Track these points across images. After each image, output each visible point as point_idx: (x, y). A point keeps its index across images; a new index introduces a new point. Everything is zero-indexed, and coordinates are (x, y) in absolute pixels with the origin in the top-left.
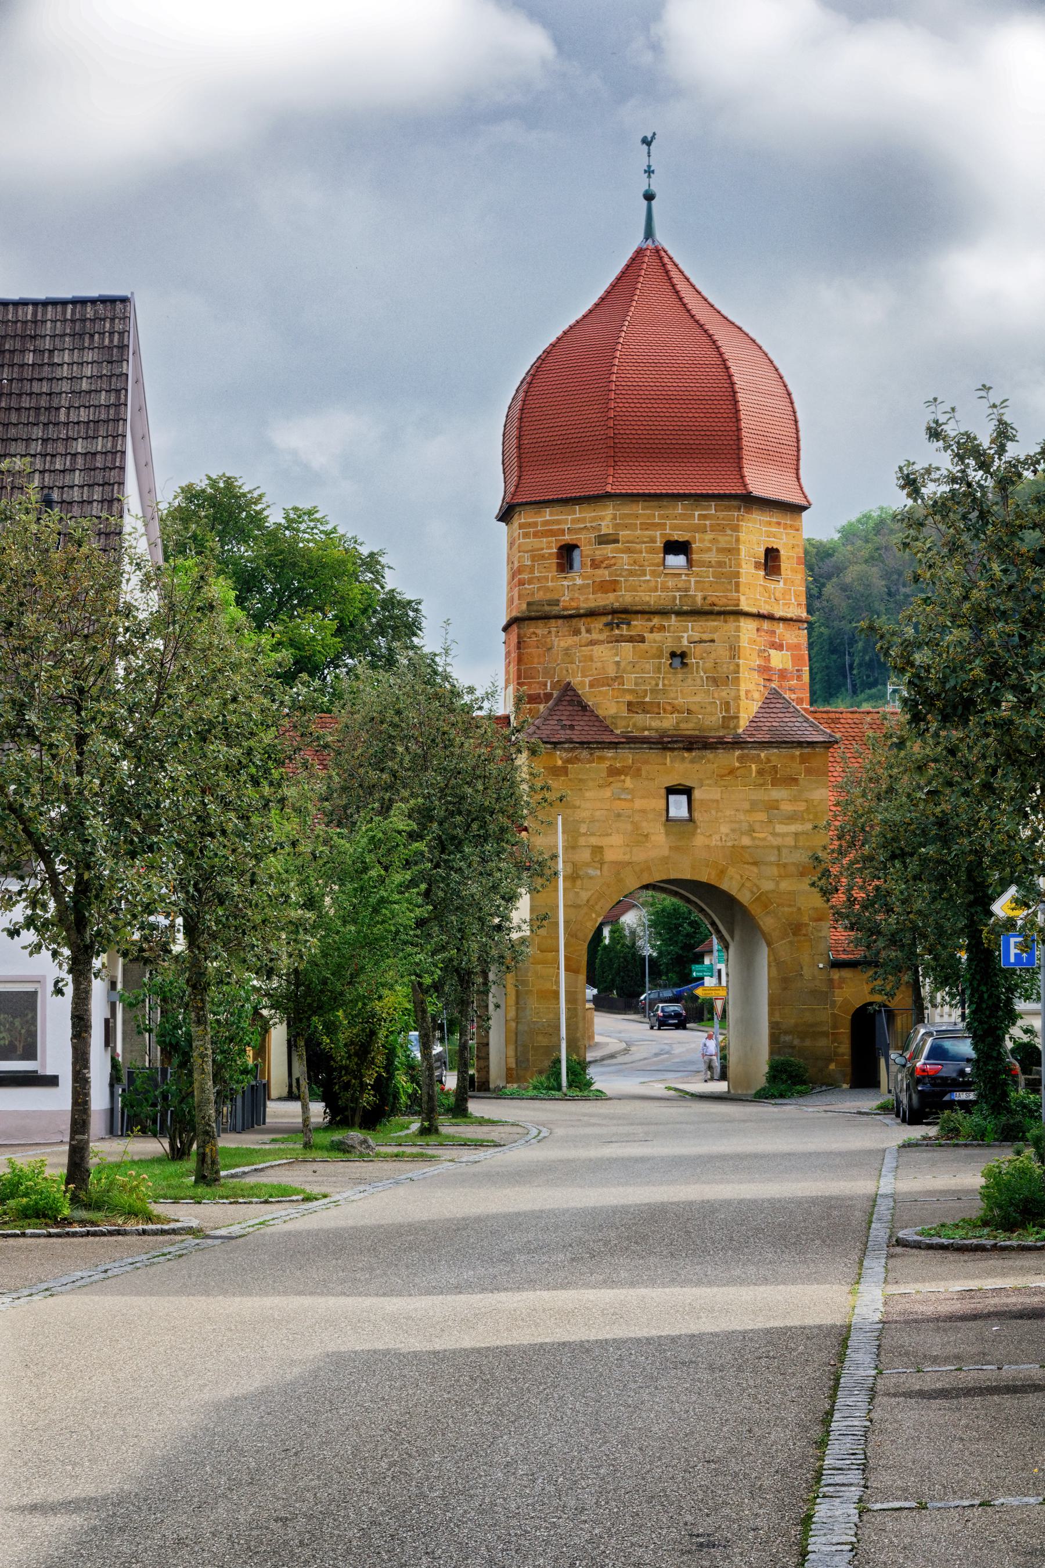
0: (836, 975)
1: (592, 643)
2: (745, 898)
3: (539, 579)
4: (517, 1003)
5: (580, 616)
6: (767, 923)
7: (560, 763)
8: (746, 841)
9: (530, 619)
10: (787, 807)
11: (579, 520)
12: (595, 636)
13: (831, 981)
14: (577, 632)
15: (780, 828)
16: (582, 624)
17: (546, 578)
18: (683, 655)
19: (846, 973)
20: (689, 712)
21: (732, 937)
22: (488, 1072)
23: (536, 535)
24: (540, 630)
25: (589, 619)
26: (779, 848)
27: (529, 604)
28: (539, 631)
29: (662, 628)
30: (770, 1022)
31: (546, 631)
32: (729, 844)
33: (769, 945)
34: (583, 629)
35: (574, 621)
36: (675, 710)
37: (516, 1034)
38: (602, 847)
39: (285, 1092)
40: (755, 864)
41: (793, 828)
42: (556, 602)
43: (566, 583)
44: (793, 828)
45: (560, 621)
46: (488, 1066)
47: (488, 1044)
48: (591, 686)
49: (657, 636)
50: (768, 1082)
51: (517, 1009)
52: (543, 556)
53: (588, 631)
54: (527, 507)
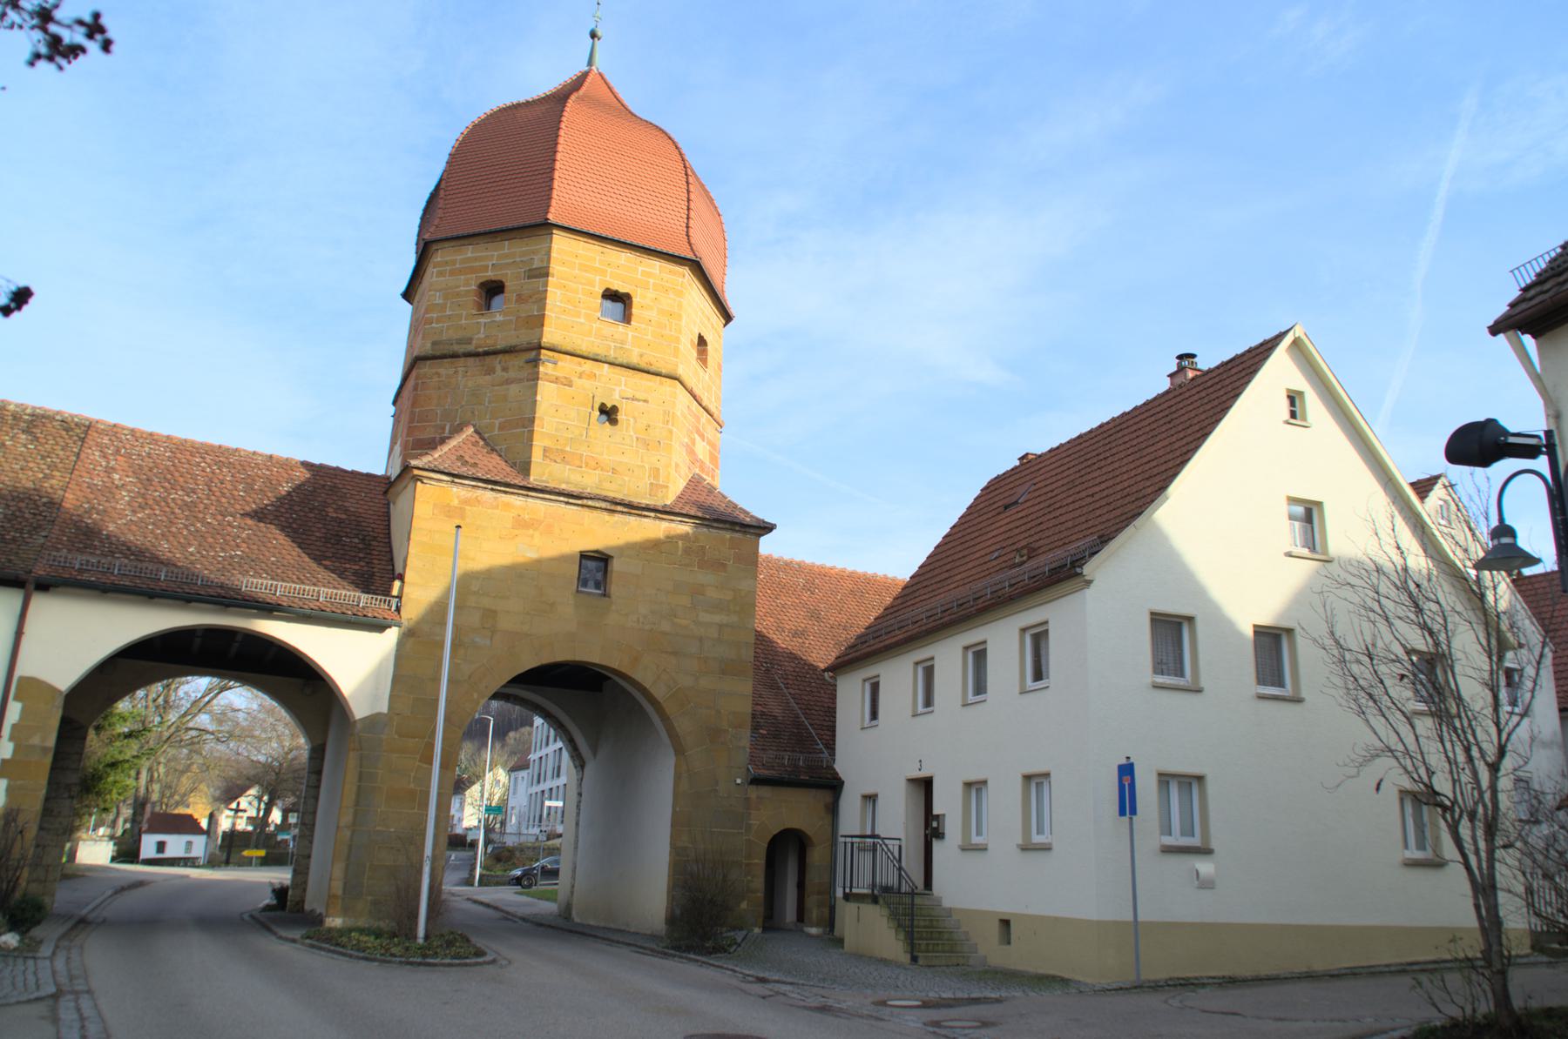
0: (754, 792)
1: (508, 382)
2: (659, 692)
3: (449, 317)
4: (357, 804)
5: (495, 353)
6: (683, 725)
7: (456, 502)
8: (665, 626)
9: (434, 358)
10: (712, 594)
11: (506, 256)
12: (512, 374)
13: (747, 799)
14: (491, 371)
15: (705, 617)
16: (496, 362)
17: (460, 317)
18: (615, 409)
19: (765, 791)
20: (614, 471)
21: (595, 751)
22: (305, 890)
23: (452, 273)
24: (445, 369)
25: (507, 357)
26: (701, 639)
27: (434, 343)
28: (442, 371)
29: (593, 376)
30: (673, 846)
31: (451, 371)
32: (647, 627)
33: (679, 750)
34: (498, 368)
35: (488, 359)
36: (598, 465)
37: (350, 847)
38: (495, 612)
39: (818, 798)
40: (675, 653)
41: (717, 618)
42: (469, 341)
43: (482, 320)
44: (717, 618)
45: (470, 360)
46: (305, 883)
47: (309, 857)
48: (501, 428)
49: (585, 382)
50: (671, 920)
51: (356, 814)
52: (458, 294)
53: (505, 369)
54: (446, 244)
